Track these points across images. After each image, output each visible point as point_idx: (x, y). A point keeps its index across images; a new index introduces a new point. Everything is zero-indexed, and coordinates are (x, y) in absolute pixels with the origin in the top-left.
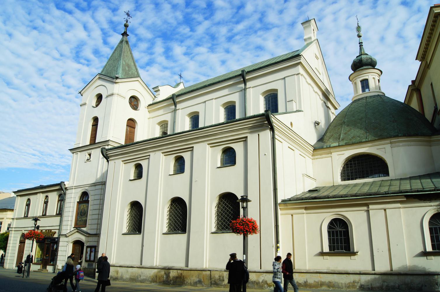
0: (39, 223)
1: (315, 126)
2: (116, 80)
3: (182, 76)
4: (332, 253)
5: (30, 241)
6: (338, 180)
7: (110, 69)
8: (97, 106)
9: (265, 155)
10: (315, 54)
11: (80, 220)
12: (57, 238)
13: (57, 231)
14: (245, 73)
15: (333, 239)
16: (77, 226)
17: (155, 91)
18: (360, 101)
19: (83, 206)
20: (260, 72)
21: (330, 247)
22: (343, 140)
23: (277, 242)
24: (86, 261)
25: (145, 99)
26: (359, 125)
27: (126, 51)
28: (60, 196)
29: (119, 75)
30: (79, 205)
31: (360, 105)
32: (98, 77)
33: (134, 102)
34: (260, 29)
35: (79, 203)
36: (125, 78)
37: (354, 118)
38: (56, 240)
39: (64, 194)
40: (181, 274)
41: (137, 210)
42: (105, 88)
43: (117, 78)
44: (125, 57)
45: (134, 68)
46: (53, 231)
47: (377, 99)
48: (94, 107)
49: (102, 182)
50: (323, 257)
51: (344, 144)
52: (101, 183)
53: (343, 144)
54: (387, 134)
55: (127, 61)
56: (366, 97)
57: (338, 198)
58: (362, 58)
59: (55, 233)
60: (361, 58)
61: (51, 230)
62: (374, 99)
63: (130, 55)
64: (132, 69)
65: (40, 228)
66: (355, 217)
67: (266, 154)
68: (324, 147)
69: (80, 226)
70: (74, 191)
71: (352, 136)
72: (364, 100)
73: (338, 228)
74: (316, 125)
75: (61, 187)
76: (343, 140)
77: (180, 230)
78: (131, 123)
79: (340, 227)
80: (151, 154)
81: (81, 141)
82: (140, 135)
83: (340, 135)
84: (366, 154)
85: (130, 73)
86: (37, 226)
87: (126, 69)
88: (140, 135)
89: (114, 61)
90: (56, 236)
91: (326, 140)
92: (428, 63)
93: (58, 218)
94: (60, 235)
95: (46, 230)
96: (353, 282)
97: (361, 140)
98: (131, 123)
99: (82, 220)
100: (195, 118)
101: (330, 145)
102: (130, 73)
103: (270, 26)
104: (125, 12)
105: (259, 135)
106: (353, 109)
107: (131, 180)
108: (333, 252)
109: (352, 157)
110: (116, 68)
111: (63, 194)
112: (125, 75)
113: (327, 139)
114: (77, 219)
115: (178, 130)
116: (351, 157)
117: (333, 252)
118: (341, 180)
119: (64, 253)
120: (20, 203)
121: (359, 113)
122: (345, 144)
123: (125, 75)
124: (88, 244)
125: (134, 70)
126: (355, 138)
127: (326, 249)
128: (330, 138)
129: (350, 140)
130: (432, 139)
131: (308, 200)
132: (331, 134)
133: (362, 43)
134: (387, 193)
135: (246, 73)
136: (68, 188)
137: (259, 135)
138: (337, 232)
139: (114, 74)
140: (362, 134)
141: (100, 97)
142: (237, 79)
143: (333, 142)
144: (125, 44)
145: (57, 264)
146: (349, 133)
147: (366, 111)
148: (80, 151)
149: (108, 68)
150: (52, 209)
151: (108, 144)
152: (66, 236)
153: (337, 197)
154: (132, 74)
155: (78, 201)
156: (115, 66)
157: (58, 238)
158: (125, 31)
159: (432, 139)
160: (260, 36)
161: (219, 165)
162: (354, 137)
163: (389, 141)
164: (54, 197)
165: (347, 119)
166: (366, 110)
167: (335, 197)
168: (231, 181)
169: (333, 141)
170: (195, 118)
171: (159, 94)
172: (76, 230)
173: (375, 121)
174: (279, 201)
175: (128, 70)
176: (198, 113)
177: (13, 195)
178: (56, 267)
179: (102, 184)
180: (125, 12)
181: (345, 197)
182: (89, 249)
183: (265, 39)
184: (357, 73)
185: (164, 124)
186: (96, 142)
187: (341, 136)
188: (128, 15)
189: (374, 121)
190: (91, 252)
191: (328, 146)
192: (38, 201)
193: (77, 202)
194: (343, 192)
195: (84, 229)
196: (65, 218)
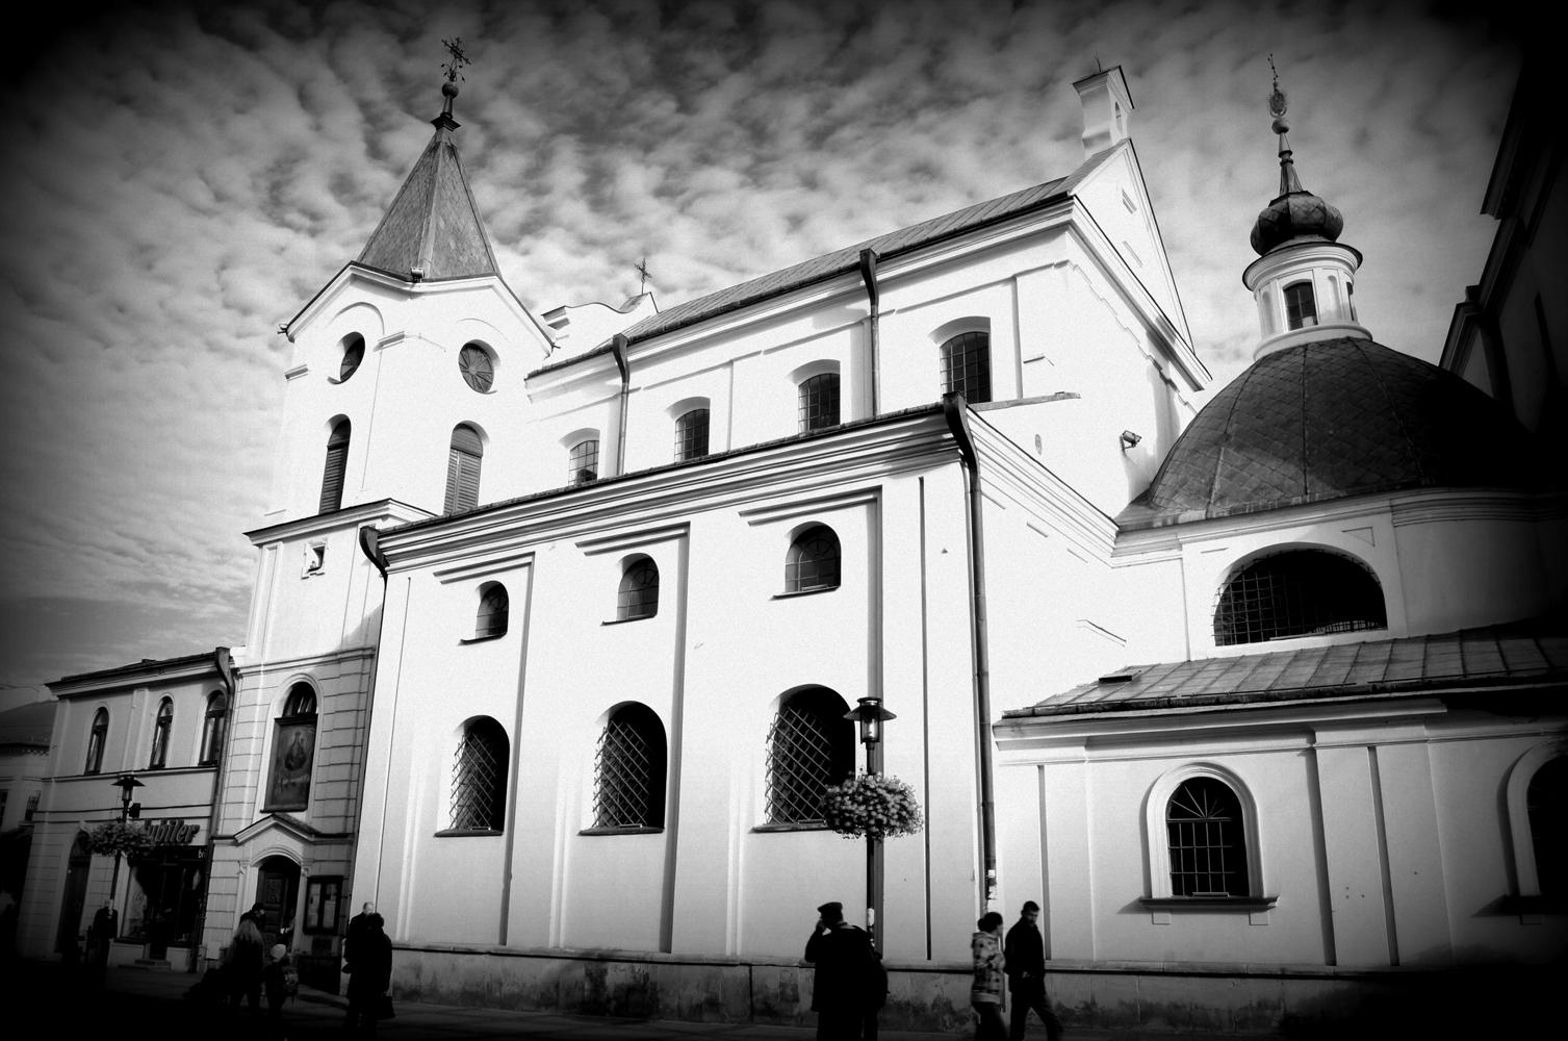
1: (1123, 449)
2: (412, 286)
3: (647, 270)
6: (1205, 645)
7: (392, 246)
8: (345, 377)
11: (286, 785)
12: (202, 848)
13: (203, 824)
14: (872, 260)
16: (274, 807)
19: (298, 734)
21: (1176, 879)
22: (1221, 498)
24: (307, 930)
27: (450, 184)
31: (1282, 375)
32: (348, 273)
34: (927, 104)
35: (282, 723)
36: (444, 276)
38: (201, 854)
41: (487, 746)
42: (377, 316)
43: (417, 278)
46: (187, 823)
49: (363, 649)
51: (1226, 514)
52: (360, 653)
53: (1221, 515)
56: (1305, 347)
59: (196, 830)
64: (470, 246)
65: (141, 812)
68: (1155, 525)
69: (286, 807)
71: (1254, 485)
72: (1295, 355)
73: (1196, 817)
74: (1127, 444)
76: (1221, 498)
83: (1211, 483)
85: (464, 259)
87: (449, 244)
89: (406, 217)
90: (199, 840)
91: (1163, 501)
92: (1527, 221)
93: (208, 778)
94: (213, 837)
96: (1259, 1004)
97: (1287, 500)
99: (294, 784)
102: (464, 259)
103: (964, 95)
105: (921, 480)
107: (465, 643)
110: (412, 242)
111: (225, 693)
113: (1166, 495)
114: (275, 780)
121: (1280, 401)
122: (1230, 512)
124: (315, 871)
125: (478, 252)
128: (1176, 492)
129: (1249, 498)
132: (1180, 477)
133: (1290, 153)
136: (242, 671)
137: (921, 480)
139: (405, 264)
141: (355, 347)
142: (844, 281)
143: (1186, 506)
144: (447, 156)
147: (1306, 396)
148: (284, 540)
149: (383, 243)
150: (188, 743)
152: (234, 841)
154: (471, 263)
155: (280, 716)
157: (208, 849)
160: (927, 130)
161: (782, 591)
163: (1387, 503)
164: (191, 703)
165: (1235, 425)
166: (1304, 393)
168: (823, 645)
172: (272, 821)
174: (995, 716)
175: (457, 250)
178: (201, 952)
179: (364, 657)
182: (316, 889)
183: (943, 141)
186: (342, 508)
187: (1217, 486)
189: (1331, 432)
190: (324, 897)
193: (276, 719)
195: (300, 817)
196: (230, 779)
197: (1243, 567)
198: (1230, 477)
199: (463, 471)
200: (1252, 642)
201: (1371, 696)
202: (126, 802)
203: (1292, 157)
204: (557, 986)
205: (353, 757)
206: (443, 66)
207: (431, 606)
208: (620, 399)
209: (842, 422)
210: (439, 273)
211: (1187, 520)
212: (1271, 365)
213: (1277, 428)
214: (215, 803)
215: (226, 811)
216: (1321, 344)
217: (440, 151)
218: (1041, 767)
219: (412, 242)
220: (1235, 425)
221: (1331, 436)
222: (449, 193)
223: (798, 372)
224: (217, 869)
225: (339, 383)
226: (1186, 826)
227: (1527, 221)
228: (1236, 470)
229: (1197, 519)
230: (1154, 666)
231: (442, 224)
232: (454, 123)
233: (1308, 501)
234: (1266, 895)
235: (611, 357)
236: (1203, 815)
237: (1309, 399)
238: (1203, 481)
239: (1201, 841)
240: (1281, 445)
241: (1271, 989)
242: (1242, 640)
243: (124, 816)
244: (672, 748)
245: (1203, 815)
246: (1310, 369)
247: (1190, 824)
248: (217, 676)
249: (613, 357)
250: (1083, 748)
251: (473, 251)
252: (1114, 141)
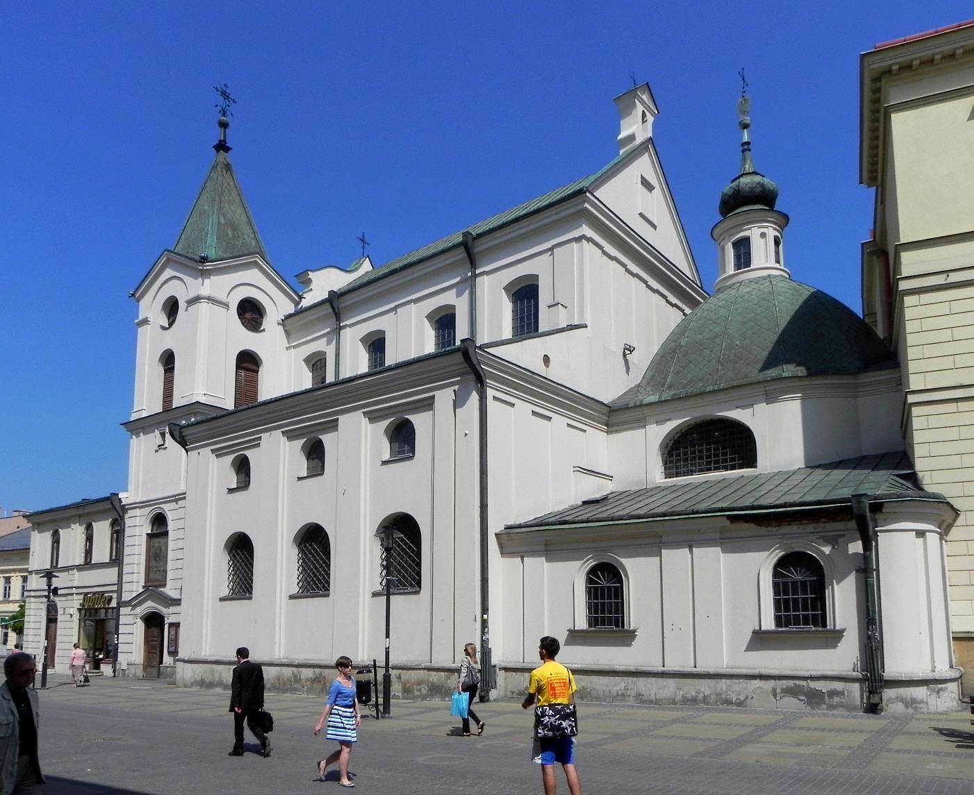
0: (56, 583)
3: (361, 243)
6: (657, 475)
7: (193, 236)
8: (171, 325)
9: (466, 435)
13: (115, 595)
14: (470, 240)
15: (596, 604)
16: (149, 584)
17: (495, 398)
20: (546, 218)
22: (669, 387)
23: (485, 610)
25: (277, 306)
27: (227, 191)
28: (113, 524)
29: (211, 253)
30: (150, 541)
33: (251, 313)
35: (150, 536)
36: (225, 256)
37: (700, 336)
39: (121, 519)
40: (321, 674)
41: (240, 547)
43: (204, 260)
44: (224, 206)
45: (248, 230)
47: (762, 287)
48: (164, 328)
51: (670, 398)
53: (666, 399)
55: (228, 215)
58: (741, 184)
59: (111, 598)
60: (738, 186)
61: (103, 593)
62: (756, 286)
63: (238, 198)
64: (243, 234)
65: (59, 591)
67: (467, 432)
68: (630, 406)
70: (138, 512)
71: (689, 379)
73: (604, 580)
74: (627, 352)
75: (112, 503)
76: (669, 387)
77: (321, 590)
78: (248, 362)
80: (437, 393)
81: (145, 404)
82: (272, 385)
83: (666, 378)
85: (239, 243)
86: (52, 587)
87: (228, 235)
88: (272, 385)
90: (114, 604)
93: (114, 571)
94: (120, 604)
95: (94, 593)
98: (248, 362)
100: (376, 344)
101: (642, 401)
102: (239, 243)
104: (217, 90)
107: (300, 479)
108: (595, 629)
109: (689, 426)
110: (203, 233)
111: (119, 519)
112: (225, 251)
115: (346, 373)
116: (687, 424)
117: (593, 629)
118: (665, 474)
119: (66, 639)
120: (40, 543)
121: (715, 322)
122: (672, 397)
123: (225, 251)
125: (248, 236)
126: (693, 383)
127: (769, 623)
129: (684, 387)
130: (861, 381)
134: (695, 511)
135: (474, 239)
138: (794, 583)
140: (709, 374)
141: (172, 308)
143: (651, 393)
144: (225, 172)
145: (119, 659)
150: (102, 552)
151: (196, 410)
152: (127, 604)
156: (204, 229)
158: (222, 139)
159: (861, 381)
161: (387, 456)
162: (693, 381)
164: (102, 529)
168: (405, 490)
169: (652, 391)
170: (376, 344)
171: (311, 290)
173: (740, 343)
174: (495, 526)
176: (384, 332)
177: (25, 524)
180: (217, 90)
184: (729, 223)
185: (316, 363)
187: (669, 379)
188: (225, 95)
189: (738, 343)
191: (638, 404)
192: (73, 537)
194: (676, 504)
196: (126, 569)
197: (681, 430)
198: (677, 373)
199: (247, 381)
200: (730, 470)
202: (49, 585)
203: (750, 146)
204: (279, 680)
206: (216, 106)
207: (213, 468)
208: (470, 281)
209: (327, 382)
210: (221, 254)
211: (648, 402)
213: (708, 341)
214: (120, 583)
215: (125, 587)
217: (219, 168)
219: (203, 233)
221: (737, 345)
222: (227, 198)
223: (507, 289)
224: (122, 620)
225: (168, 329)
226: (785, 584)
228: (681, 369)
229: (653, 401)
231: (222, 220)
232: (227, 147)
233: (716, 389)
234: (838, 628)
235: (328, 305)
236: (603, 582)
237: (730, 321)
240: (708, 352)
241: (82, 630)
242: (678, 475)
243: (49, 593)
245: (603, 582)
248: (114, 510)
249: (464, 250)
251: (246, 237)
252: (638, 141)
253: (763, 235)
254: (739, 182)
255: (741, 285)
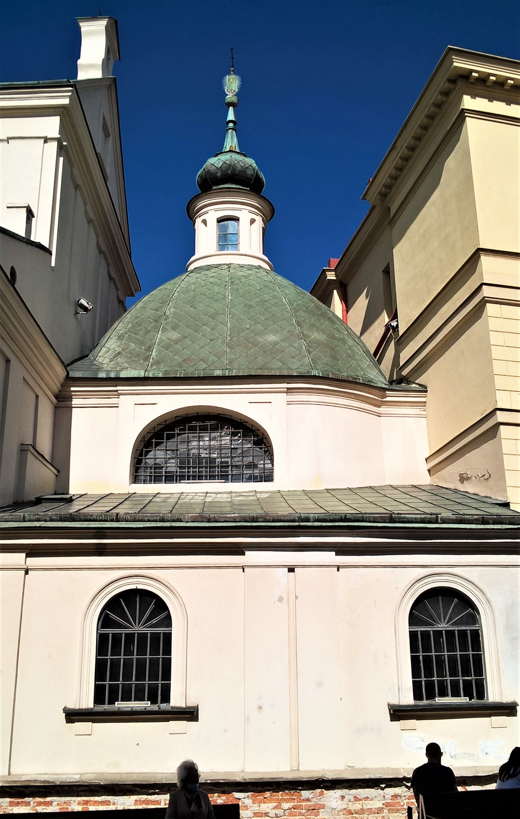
4: (424, 709)
5: (166, 795)
10: (104, 119)
18: (213, 270)
21: (417, 686)
26: (209, 329)
31: (211, 280)
46: (486, 299)
47: (259, 275)
50: (188, 705)
54: (281, 364)
56: (229, 265)
57: (149, 521)
62: (250, 272)
66: (184, 584)
71: (185, 357)
76: (157, 363)
79: (442, 619)
84: (216, 412)
92: (393, 212)
97: (210, 371)
106: (193, 287)
131: (46, 521)
143: (127, 365)
146: (178, 346)
153: (146, 519)
165: (173, 310)
167: (140, 518)
181: (173, 521)
189: (248, 327)
201: (297, 524)
205: (400, 700)
212: (202, 273)
216: (242, 266)
218: (27, 573)
220: (173, 310)
227: (393, 212)
230: (82, 496)
238: (143, 348)
239: (439, 648)
244: (352, 536)
246: (233, 280)
247: (428, 632)
250: (334, 553)
253: (253, 221)
254: (231, 156)
255: (230, 267)
